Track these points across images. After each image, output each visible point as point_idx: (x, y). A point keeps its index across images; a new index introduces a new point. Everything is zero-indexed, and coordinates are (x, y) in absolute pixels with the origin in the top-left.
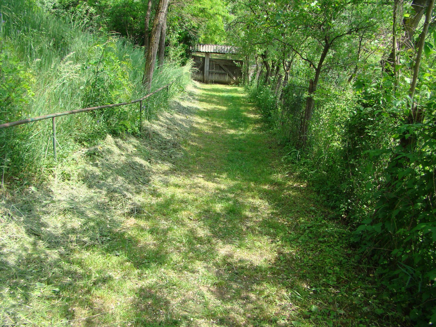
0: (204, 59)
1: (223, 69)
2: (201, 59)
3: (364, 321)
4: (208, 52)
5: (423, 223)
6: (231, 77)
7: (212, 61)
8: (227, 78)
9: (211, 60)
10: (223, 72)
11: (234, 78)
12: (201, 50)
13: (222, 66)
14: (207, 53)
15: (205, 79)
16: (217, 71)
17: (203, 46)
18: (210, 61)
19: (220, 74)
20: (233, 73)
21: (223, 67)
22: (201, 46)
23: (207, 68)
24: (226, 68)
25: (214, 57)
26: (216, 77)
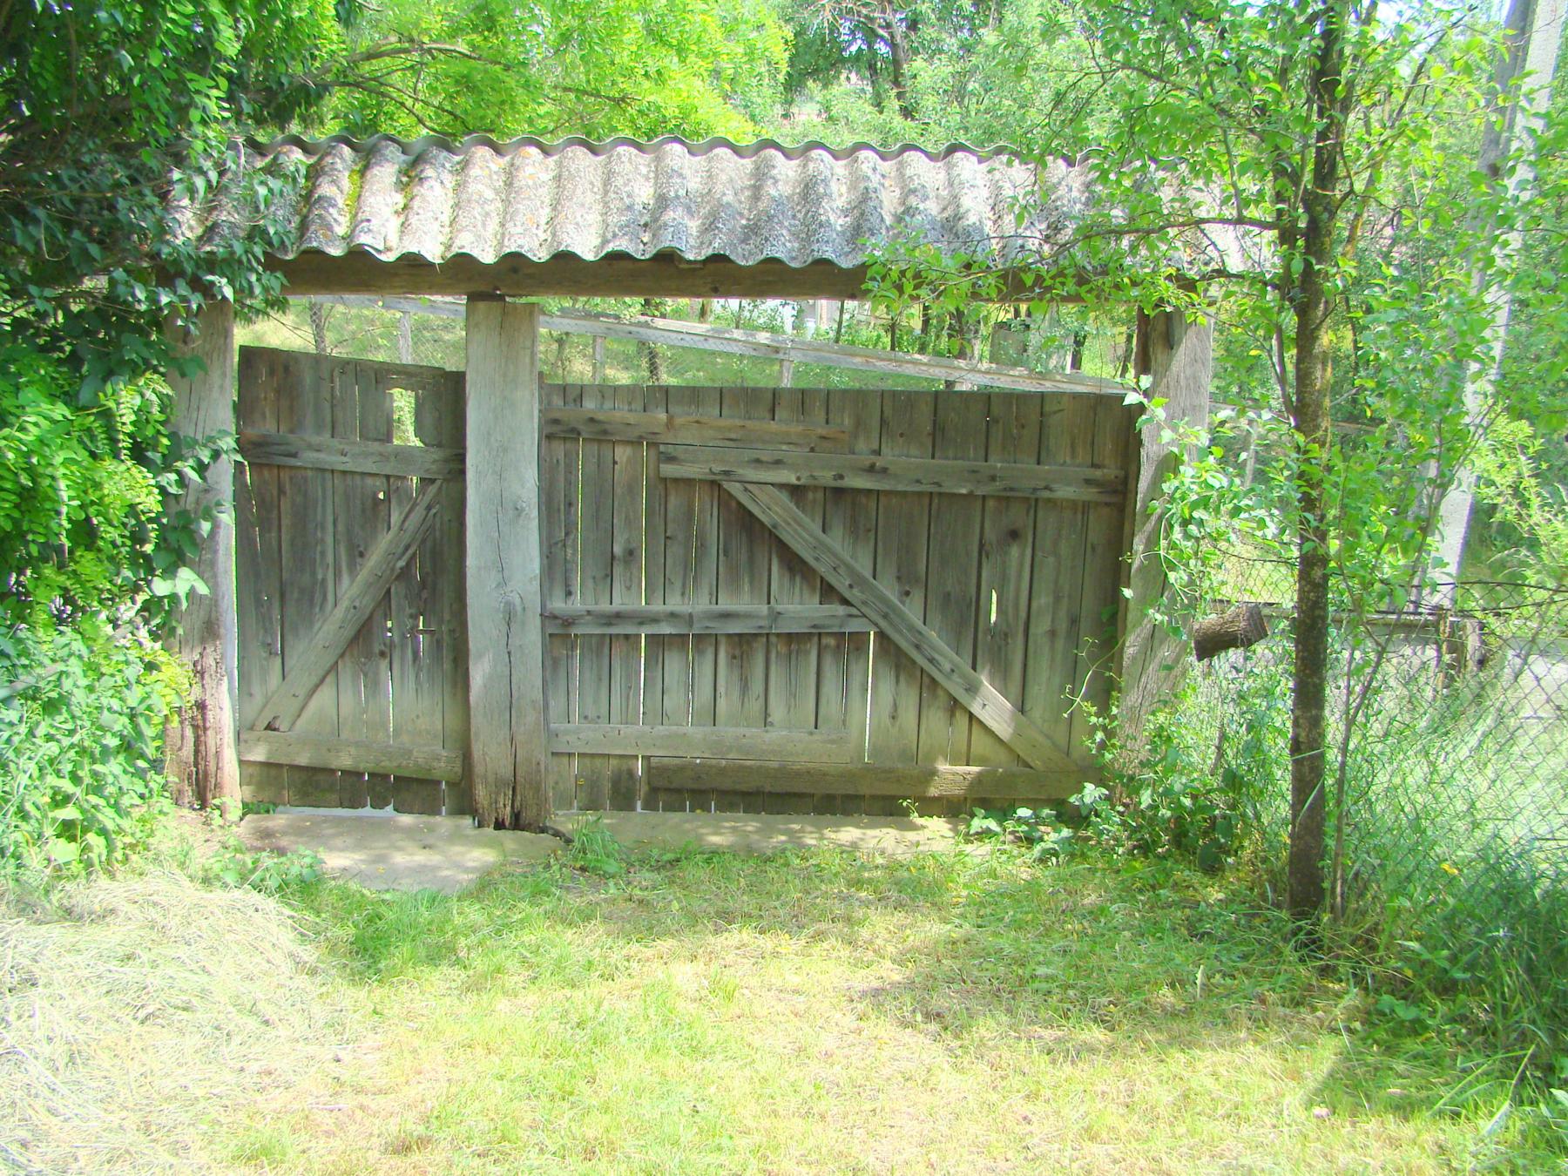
0: (445, 395)
1: (795, 565)
2: (403, 402)
3: (158, 743)
4: (514, 263)
5: (1301, 591)
6: (929, 685)
7: (602, 434)
8: (866, 714)
9: (569, 425)
10: (800, 608)
11: (993, 706)
12: (386, 237)
13: (773, 509)
14: (498, 286)
15: (491, 754)
16: (699, 604)
17: (411, 174)
18: (556, 431)
19: (742, 643)
20: (963, 615)
21: (801, 530)
22: (385, 173)
23: (505, 562)
24: (837, 540)
25: (587, 346)
26: (680, 714)
